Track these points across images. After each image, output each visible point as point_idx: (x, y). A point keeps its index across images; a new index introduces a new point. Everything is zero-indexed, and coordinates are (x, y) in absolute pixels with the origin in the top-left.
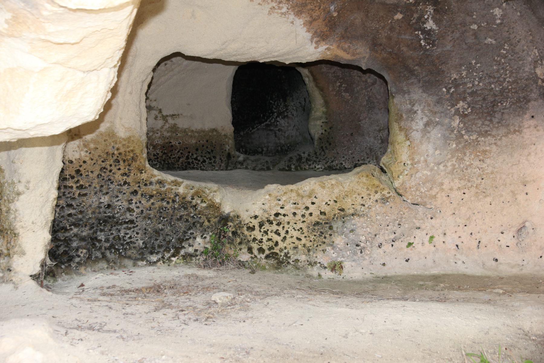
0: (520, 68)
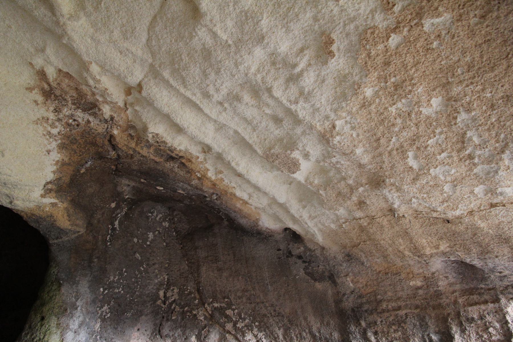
0: (146, 286)
